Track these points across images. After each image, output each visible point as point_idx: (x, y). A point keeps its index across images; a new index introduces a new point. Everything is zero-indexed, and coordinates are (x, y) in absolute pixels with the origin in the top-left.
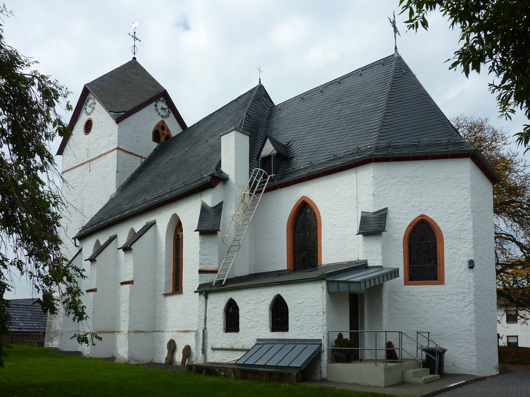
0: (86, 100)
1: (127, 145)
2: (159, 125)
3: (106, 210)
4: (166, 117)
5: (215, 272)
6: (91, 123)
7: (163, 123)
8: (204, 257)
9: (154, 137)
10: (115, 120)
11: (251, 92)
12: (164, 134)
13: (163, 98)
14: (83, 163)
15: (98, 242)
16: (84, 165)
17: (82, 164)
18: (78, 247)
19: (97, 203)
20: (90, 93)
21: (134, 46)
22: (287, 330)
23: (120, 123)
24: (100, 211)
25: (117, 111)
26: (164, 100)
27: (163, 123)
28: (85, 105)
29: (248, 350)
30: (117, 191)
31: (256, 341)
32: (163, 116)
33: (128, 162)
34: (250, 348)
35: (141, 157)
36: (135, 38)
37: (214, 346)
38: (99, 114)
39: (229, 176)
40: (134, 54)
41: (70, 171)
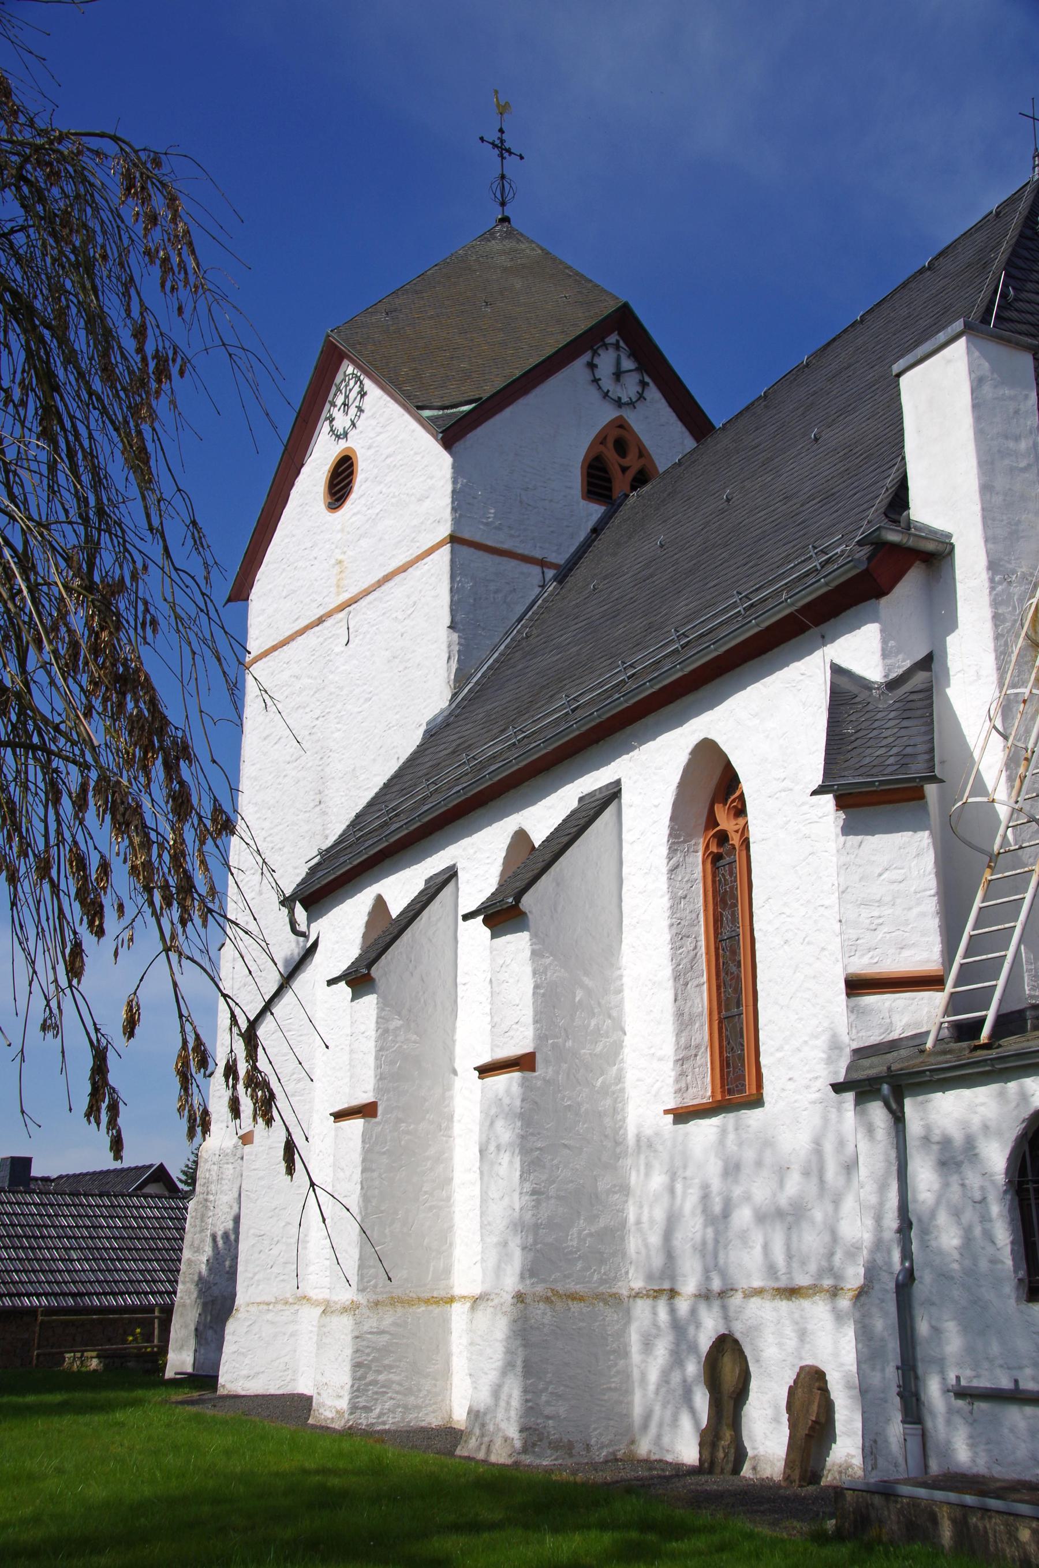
0: (334, 389)
2: (605, 438)
3: (410, 777)
4: (632, 404)
6: (352, 465)
7: (621, 426)
8: (865, 913)
9: (589, 484)
10: (441, 435)
11: (998, 214)
12: (628, 468)
13: (619, 334)
14: (321, 617)
15: (380, 903)
16: (325, 624)
17: (320, 621)
18: (303, 935)
19: (374, 760)
20: (346, 362)
23: (459, 446)
24: (386, 786)
25: (447, 403)
26: (622, 344)
27: (621, 426)
28: (327, 406)
30: (452, 701)
32: (619, 403)
33: (492, 587)
36: (503, 150)
37: (970, 1379)
38: (378, 429)
39: (949, 536)
40: (503, 204)
41: (276, 653)
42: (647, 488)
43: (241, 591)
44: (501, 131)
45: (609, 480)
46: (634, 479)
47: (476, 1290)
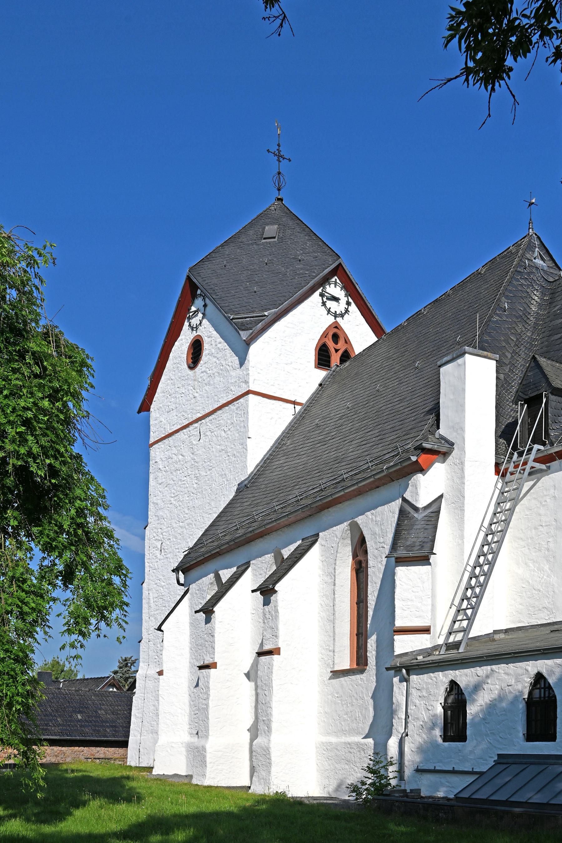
1: (268, 383)
5: (426, 630)
9: (319, 359)
21: (279, 173)
22: (553, 738)
27: (336, 327)
29: (481, 774)
31: (496, 758)
32: (336, 315)
34: (485, 770)
35: (294, 403)
36: (280, 157)
40: (279, 190)
42: (347, 364)
43: (145, 407)
44: (279, 145)
45: (329, 357)
46: (342, 356)
47: (459, 364)
